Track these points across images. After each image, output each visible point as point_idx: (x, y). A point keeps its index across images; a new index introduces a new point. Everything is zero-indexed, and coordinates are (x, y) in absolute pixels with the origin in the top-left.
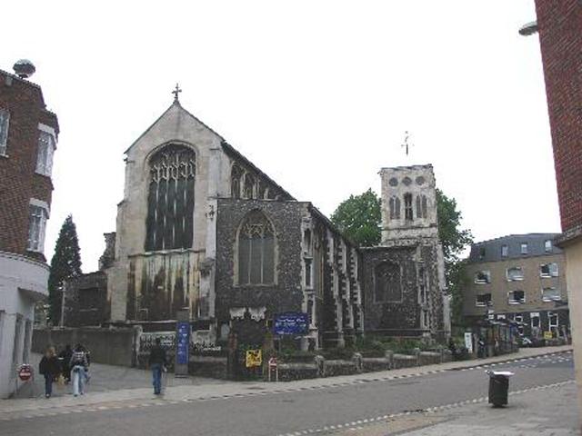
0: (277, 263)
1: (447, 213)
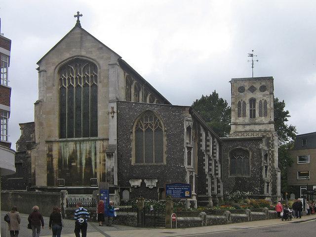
0: (165, 149)
1: (280, 114)
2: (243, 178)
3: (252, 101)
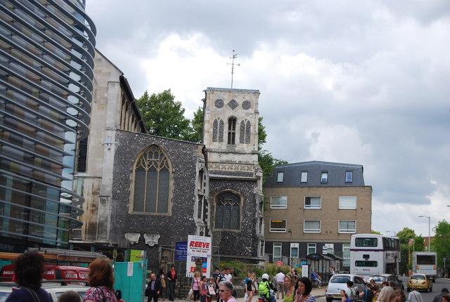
0: (171, 196)
2: (232, 233)
3: (232, 121)
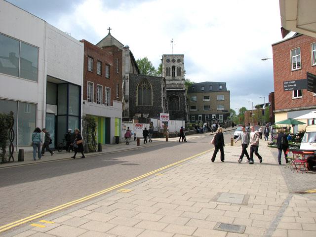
0: (152, 98)
